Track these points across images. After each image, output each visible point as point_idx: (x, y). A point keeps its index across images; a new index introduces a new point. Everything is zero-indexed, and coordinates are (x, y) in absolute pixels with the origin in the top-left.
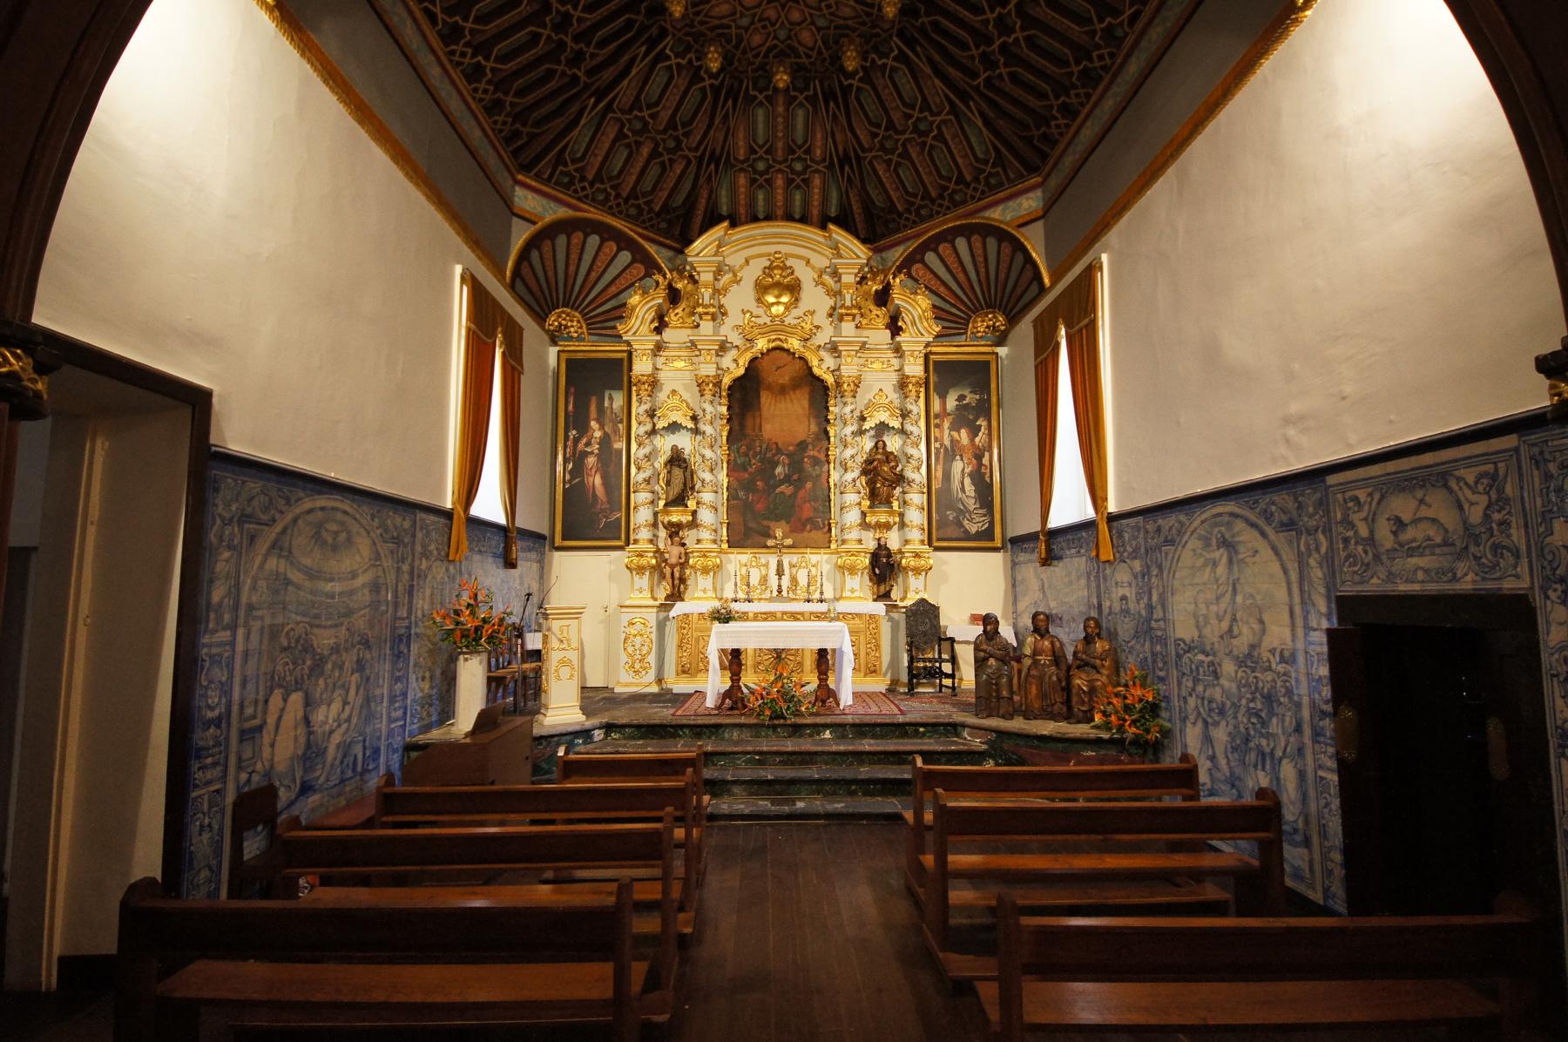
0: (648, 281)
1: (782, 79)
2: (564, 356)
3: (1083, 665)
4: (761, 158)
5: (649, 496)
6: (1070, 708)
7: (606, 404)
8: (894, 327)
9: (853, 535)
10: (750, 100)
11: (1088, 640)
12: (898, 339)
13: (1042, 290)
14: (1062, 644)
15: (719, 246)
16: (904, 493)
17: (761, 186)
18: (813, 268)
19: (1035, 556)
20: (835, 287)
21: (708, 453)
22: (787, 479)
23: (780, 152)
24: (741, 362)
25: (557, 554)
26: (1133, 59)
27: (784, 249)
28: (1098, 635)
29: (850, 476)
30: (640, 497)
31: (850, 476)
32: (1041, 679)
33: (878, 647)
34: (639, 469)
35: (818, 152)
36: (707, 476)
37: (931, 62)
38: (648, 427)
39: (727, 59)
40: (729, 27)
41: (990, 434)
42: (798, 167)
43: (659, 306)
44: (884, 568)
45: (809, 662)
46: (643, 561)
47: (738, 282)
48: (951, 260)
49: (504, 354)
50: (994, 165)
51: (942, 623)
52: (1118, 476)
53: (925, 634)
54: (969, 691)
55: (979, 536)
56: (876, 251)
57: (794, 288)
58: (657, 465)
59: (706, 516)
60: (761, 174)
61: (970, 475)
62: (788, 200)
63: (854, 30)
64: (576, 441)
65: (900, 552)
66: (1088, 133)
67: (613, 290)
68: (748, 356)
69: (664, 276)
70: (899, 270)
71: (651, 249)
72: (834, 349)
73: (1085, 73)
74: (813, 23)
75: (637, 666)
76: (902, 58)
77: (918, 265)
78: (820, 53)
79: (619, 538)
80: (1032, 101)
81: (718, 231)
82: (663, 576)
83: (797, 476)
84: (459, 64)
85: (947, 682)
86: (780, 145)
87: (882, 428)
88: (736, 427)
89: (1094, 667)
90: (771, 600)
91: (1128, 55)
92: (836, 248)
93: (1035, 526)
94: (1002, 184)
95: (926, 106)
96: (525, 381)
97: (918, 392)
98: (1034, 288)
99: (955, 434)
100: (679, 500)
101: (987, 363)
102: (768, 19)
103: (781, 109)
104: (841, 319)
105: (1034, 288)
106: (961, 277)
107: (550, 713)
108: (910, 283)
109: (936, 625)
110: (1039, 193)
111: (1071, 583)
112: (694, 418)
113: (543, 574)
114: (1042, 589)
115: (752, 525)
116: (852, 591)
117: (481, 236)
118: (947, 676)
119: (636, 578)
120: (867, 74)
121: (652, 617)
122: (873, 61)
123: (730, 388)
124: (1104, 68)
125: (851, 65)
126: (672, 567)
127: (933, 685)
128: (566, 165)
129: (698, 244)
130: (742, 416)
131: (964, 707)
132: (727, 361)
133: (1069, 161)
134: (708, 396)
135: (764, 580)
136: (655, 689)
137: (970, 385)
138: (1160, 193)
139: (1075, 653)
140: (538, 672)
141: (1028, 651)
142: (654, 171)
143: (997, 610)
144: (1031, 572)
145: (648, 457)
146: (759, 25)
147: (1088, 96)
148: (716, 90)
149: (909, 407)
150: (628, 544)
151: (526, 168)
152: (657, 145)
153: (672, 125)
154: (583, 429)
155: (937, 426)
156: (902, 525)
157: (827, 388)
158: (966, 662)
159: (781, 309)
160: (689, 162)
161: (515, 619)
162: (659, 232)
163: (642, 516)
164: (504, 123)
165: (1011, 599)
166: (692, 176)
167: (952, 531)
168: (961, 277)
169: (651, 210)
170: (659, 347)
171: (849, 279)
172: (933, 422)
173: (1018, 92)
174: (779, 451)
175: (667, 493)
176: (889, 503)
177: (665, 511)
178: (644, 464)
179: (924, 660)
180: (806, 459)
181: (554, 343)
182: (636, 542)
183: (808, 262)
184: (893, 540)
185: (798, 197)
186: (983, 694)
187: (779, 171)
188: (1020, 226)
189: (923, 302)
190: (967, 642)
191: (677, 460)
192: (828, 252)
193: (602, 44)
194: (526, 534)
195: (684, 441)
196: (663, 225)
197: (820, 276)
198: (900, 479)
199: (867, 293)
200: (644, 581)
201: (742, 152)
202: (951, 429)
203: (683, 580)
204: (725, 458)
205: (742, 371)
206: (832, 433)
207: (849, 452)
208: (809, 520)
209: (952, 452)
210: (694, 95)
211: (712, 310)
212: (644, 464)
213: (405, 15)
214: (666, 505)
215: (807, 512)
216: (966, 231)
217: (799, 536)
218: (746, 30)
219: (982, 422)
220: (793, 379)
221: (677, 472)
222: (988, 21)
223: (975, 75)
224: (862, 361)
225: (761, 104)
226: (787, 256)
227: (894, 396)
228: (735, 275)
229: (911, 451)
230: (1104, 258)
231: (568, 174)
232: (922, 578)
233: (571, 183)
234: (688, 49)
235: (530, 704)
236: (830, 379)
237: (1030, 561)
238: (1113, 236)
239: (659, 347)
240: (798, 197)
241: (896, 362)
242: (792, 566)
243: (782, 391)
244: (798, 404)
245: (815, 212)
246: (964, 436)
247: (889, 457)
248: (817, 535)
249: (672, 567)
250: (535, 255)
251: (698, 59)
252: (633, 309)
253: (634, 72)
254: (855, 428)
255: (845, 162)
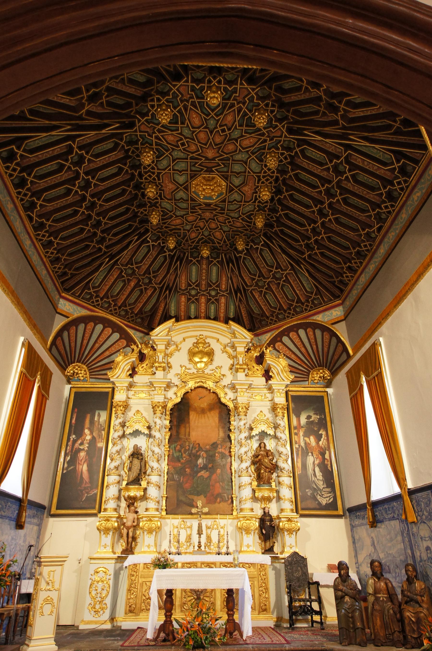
0: (128, 349)
1: (206, 253)
2: (74, 390)
3: (409, 601)
4: (193, 289)
5: (117, 478)
6: (405, 637)
7: (96, 418)
8: (267, 375)
9: (248, 505)
10: (189, 262)
11: (410, 581)
12: (270, 382)
13: (349, 357)
14: (393, 587)
15: (169, 331)
16: (278, 476)
17: (193, 302)
18: (221, 344)
19: (366, 521)
20: (234, 354)
21: (157, 450)
22: (205, 467)
23: (203, 286)
24: (179, 394)
25: (52, 520)
26: (382, 246)
27: (205, 333)
28: (416, 576)
29: (244, 465)
30: (111, 479)
31: (244, 465)
32: (382, 612)
33: (267, 589)
34: (112, 460)
35: (224, 287)
36: (155, 465)
37: (280, 247)
38: (121, 433)
39: (178, 243)
40: (180, 229)
41: (328, 440)
42: (213, 293)
43: (133, 362)
44: (268, 530)
45: (219, 601)
46: (109, 525)
47: (179, 350)
48: (297, 341)
49: (39, 387)
50: (316, 294)
51: (310, 571)
52: (410, 464)
53: (298, 579)
54: (333, 626)
55: (328, 507)
56: (256, 335)
57: (210, 354)
58: (124, 457)
59: (153, 492)
60: (193, 296)
61: (319, 465)
62: (207, 309)
63: (242, 233)
64: (75, 441)
65: (278, 518)
66: (363, 279)
67: (107, 353)
68: (183, 391)
69: (137, 346)
70: (269, 345)
71: (131, 332)
72: (233, 388)
73: (358, 253)
74: (221, 229)
75: (97, 607)
76: (266, 245)
77: (279, 343)
78: (225, 242)
79: (94, 508)
80: (333, 266)
81: (169, 323)
82: (121, 536)
83: (211, 465)
84: (40, 240)
85: (317, 618)
86: (204, 283)
87: (263, 435)
88: (174, 433)
89: (417, 602)
90: (193, 553)
91: (378, 247)
92: (234, 334)
93: (363, 500)
94: (321, 304)
95: (279, 266)
96: (49, 404)
97: (283, 413)
98: (344, 356)
99: (307, 439)
100: (136, 481)
101: (322, 397)
102: (199, 227)
103: (204, 266)
104: (237, 371)
105: (344, 356)
106: (303, 349)
107: (32, 643)
108: (275, 352)
109: (305, 573)
110: (341, 308)
111: (391, 540)
112: (149, 428)
113: (39, 535)
114: (373, 544)
115: (182, 498)
116: (248, 546)
117: (37, 323)
118: (317, 613)
119: (103, 537)
120: (248, 252)
121: (111, 566)
122: (251, 246)
123: (171, 410)
124: (368, 250)
125: (240, 248)
126: (128, 528)
127: (306, 621)
128: (89, 289)
129: (157, 330)
130: (178, 427)
131: (331, 637)
132: (170, 394)
133: (355, 293)
134: (158, 414)
135: (189, 538)
136: (108, 626)
137: (314, 409)
138: (406, 306)
139: (402, 591)
140: (27, 611)
141: (370, 590)
142: (136, 293)
143: (346, 559)
144: (364, 532)
145: (118, 452)
146: (194, 229)
147: (361, 263)
148: (172, 257)
149: (279, 422)
150: (100, 511)
151: (67, 290)
152: (139, 281)
153: (147, 271)
154: (79, 433)
155: (296, 434)
156: (279, 499)
157: (229, 410)
158: (330, 604)
159: (203, 365)
160: (155, 289)
161: (15, 568)
162: (136, 323)
163: (111, 492)
164: (59, 268)
165: (353, 554)
166: (156, 297)
167: (311, 504)
168: (303, 349)
169: (132, 313)
170: (131, 386)
171: (241, 349)
172: (293, 431)
173: (325, 261)
174: (200, 449)
175: (129, 477)
176: (269, 483)
177: (127, 489)
178: (116, 457)
179: (300, 600)
180: (217, 454)
181: (69, 382)
182: (105, 510)
183: (218, 340)
184: (273, 509)
185: (213, 307)
186: (343, 625)
187: (203, 295)
188: (333, 324)
189: (283, 362)
190: (327, 586)
191: (136, 454)
192: (229, 335)
193: (115, 235)
194: (33, 504)
195: (141, 442)
196: (139, 320)
197: (225, 348)
198: (275, 467)
199: (252, 357)
200: (108, 539)
201: (183, 285)
202: (304, 436)
203: (134, 539)
204: (167, 453)
205: (179, 400)
206: (232, 438)
207: (243, 450)
208: (219, 495)
209: (306, 451)
210: (160, 259)
211: (163, 365)
212: (116, 457)
213: (17, 217)
214: (127, 484)
215: (218, 489)
216: (305, 326)
217: (213, 506)
218: (189, 231)
219: (322, 432)
220: (210, 405)
221: (136, 462)
222: (307, 230)
223: (303, 253)
224: (250, 395)
225: (194, 264)
226: (207, 337)
227: (269, 416)
228: (177, 346)
229: (281, 449)
230: (381, 339)
231: (90, 293)
232: (293, 536)
233: (91, 298)
234: (159, 238)
235: (17, 638)
236: (231, 405)
237: (362, 525)
238: (385, 328)
239: (131, 386)
240: (213, 307)
241: (269, 396)
242: (208, 528)
243: (203, 411)
244: (213, 419)
245: (222, 315)
246: (312, 440)
247: (268, 453)
248: (224, 506)
249: (128, 528)
250: (65, 334)
251: (163, 243)
252: (118, 363)
253: (130, 248)
254: (247, 434)
255: (238, 292)
